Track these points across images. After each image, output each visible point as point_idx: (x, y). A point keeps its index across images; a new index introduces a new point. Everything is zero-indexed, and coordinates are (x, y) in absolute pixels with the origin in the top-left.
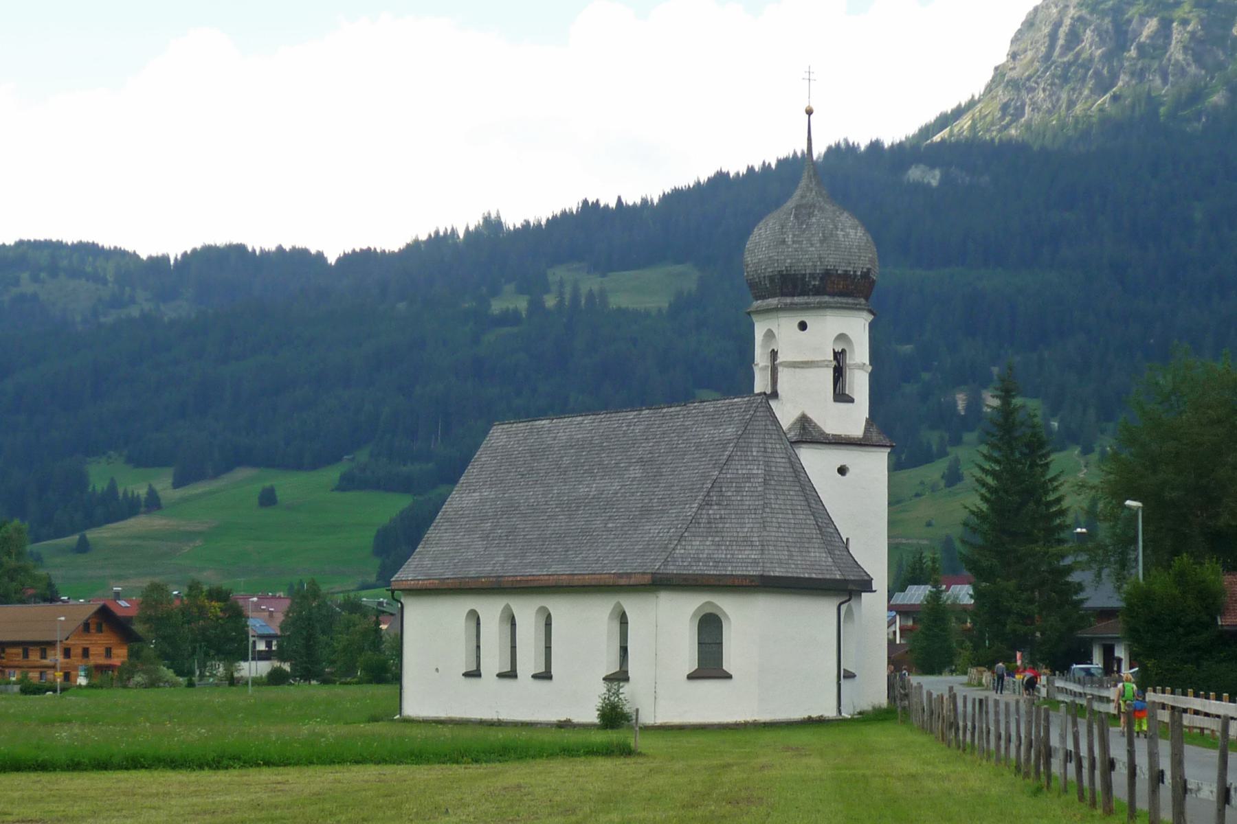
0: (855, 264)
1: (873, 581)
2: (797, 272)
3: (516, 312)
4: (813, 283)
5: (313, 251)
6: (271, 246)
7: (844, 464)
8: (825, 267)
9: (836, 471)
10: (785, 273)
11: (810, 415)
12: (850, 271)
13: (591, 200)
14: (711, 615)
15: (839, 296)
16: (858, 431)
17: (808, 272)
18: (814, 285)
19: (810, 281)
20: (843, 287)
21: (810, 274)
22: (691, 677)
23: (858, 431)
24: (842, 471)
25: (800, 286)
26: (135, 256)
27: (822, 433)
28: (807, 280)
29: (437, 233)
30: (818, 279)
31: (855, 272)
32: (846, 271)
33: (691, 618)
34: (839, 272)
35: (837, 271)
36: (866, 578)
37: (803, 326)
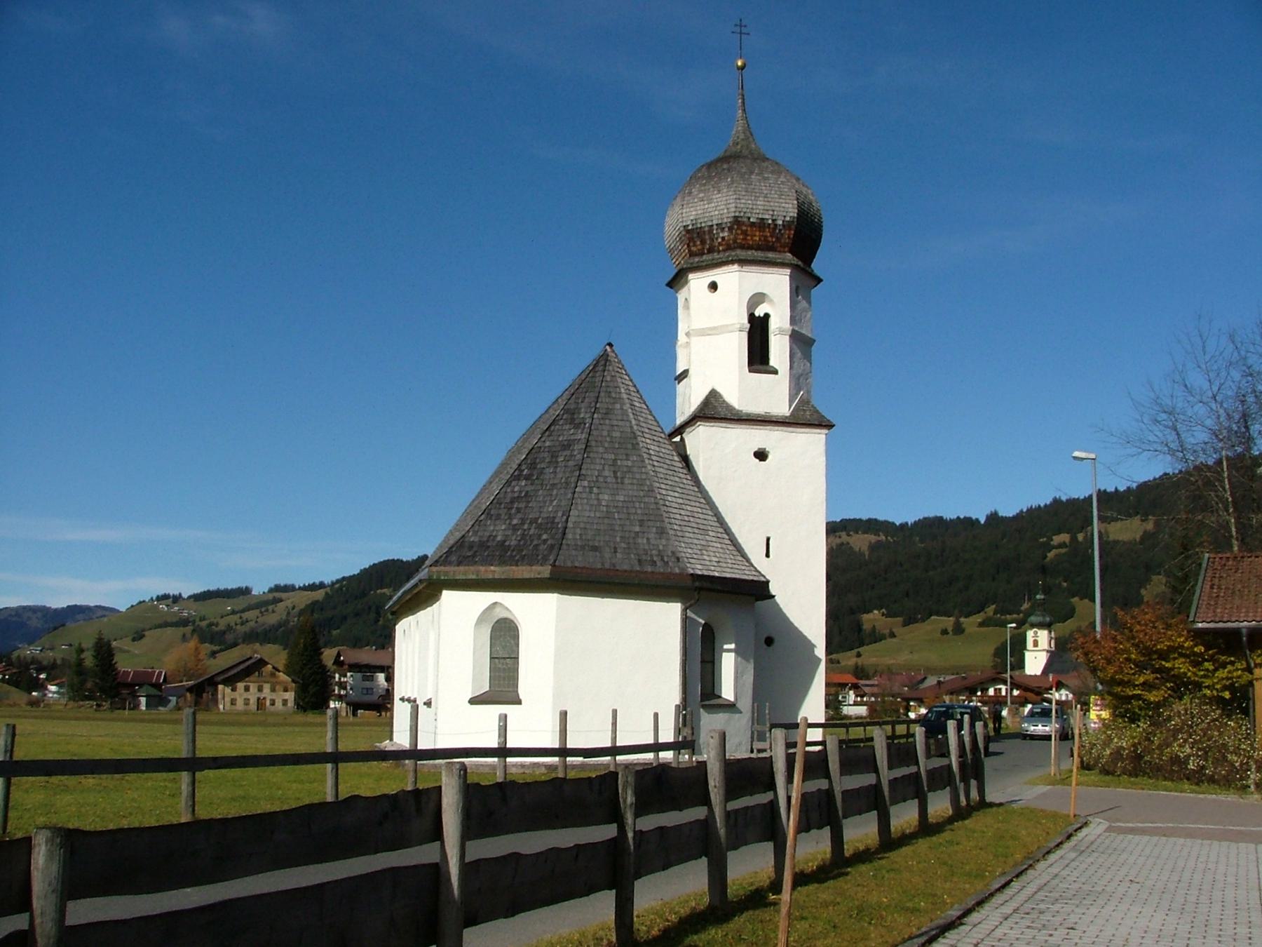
0: (773, 211)
1: (770, 584)
2: (703, 225)
3: (1064, 543)
4: (721, 235)
5: (974, 518)
6: (954, 516)
7: (764, 447)
8: (733, 215)
9: (767, 461)
10: (690, 227)
11: (719, 390)
12: (767, 219)
13: (1102, 489)
14: (505, 619)
15: (756, 250)
16: (782, 408)
17: (715, 222)
18: (723, 238)
19: (718, 233)
20: (760, 239)
21: (717, 225)
22: (474, 701)
23: (782, 408)
24: (761, 455)
25: (708, 242)
26: (893, 524)
27: (729, 407)
28: (715, 232)
29: (1031, 507)
30: (727, 229)
31: (774, 220)
32: (763, 219)
33: (476, 625)
34: (751, 220)
35: (749, 218)
36: (763, 579)
37: (713, 286)
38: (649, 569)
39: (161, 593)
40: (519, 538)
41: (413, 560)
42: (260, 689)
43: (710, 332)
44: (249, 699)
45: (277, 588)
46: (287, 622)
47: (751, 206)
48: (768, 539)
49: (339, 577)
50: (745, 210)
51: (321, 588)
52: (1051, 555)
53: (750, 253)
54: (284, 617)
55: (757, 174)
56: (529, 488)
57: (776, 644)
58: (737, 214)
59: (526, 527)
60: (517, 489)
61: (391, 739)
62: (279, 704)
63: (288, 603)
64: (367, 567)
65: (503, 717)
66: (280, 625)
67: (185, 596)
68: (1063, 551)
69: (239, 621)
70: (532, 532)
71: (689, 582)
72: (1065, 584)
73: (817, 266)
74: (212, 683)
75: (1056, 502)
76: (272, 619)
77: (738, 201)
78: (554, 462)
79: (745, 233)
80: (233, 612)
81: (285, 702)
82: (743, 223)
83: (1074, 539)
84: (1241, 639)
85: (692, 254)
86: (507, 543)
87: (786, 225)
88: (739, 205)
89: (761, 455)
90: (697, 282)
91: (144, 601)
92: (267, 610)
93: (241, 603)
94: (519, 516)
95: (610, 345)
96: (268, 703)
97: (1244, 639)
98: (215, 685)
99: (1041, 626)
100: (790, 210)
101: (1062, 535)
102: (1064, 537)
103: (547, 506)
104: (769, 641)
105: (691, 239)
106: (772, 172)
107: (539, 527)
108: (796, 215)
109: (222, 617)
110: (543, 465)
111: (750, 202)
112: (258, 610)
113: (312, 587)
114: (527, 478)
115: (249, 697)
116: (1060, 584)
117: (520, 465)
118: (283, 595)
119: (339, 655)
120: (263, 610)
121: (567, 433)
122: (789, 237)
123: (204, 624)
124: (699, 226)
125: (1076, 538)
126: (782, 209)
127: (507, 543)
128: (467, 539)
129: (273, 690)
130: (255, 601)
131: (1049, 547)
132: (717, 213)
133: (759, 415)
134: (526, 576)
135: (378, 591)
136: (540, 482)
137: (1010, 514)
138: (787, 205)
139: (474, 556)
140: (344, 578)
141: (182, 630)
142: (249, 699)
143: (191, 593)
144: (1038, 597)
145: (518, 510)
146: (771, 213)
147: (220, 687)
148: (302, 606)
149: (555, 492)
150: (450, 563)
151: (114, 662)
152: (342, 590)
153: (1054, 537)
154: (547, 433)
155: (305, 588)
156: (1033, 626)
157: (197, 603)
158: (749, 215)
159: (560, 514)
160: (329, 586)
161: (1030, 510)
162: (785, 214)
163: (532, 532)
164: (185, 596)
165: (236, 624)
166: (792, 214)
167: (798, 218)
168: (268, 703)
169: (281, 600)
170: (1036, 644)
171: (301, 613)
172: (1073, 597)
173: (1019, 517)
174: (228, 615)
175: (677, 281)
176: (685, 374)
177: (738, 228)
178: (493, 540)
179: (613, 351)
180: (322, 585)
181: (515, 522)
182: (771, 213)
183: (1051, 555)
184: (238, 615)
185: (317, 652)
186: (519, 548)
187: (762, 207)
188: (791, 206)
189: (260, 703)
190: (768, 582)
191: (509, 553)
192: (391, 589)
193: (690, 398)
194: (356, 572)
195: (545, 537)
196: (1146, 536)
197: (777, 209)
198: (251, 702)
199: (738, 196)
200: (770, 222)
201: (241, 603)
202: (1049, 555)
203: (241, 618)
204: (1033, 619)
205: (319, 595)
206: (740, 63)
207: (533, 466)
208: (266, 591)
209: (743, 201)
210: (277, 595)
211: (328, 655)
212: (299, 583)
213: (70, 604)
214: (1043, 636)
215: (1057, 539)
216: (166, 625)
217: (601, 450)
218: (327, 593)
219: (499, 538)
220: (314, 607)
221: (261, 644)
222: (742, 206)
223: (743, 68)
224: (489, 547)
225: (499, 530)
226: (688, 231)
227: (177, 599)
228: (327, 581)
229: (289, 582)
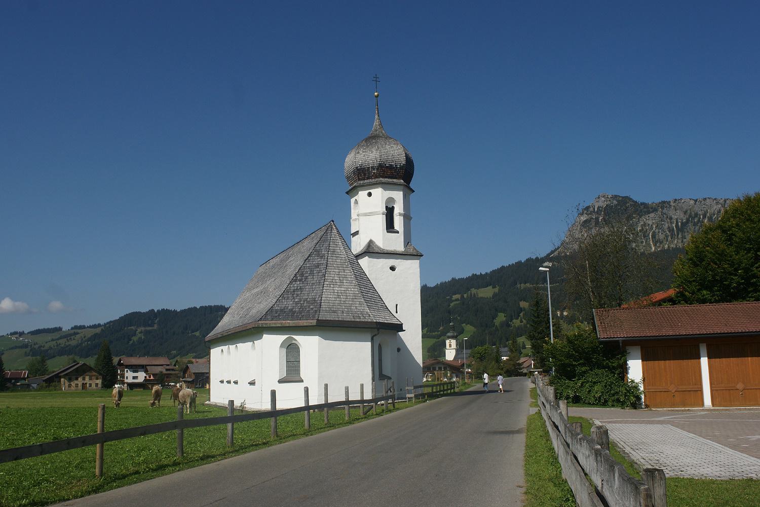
4: (373, 171)
17: (370, 166)
24: (393, 269)
38: (358, 320)
39: (13, 331)
40: (299, 308)
41: (147, 312)
42: (84, 379)
44: (78, 384)
45: (76, 327)
46: (81, 344)
48: (397, 305)
49: (108, 321)
51: (98, 327)
52: (452, 304)
53: (386, 179)
54: (80, 342)
55: (389, 145)
56: (301, 285)
57: (401, 351)
59: (302, 302)
60: (295, 285)
61: (209, 401)
62: (94, 386)
63: (82, 335)
64: (123, 316)
65: (306, 389)
66: (77, 346)
67: (26, 332)
68: (458, 302)
69: (55, 344)
70: (305, 305)
71: (375, 326)
72: (459, 318)
73: (411, 185)
74: (58, 377)
75: (453, 279)
76: (73, 343)
78: (312, 273)
79: (384, 171)
80: (53, 340)
81: (97, 385)
83: (462, 297)
84: (619, 345)
86: (294, 310)
87: (401, 168)
89: (393, 269)
90: (362, 194)
91: (3, 336)
92: (71, 339)
93: (56, 335)
94: (298, 297)
95: (333, 221)
96: (88, 385)
97: (621, 344)
98: (60, 377)
99: (453, 337)
101: (457, 295)
102: (458, 296)
103: (308, 294)
104: (399, 350)
105: (359, 173)
106: (395, 144)
107: (308, 302)
109: (46, 343)
110: (307, 275)
112: (66, 339)
113: (94, 326)
114: (300, 280)
115: (78, 383)
116: (457, 317)
117: (296, 275)
118: (79, 331)
119: (120, 360)
120: (68, 338)
121: (317, 260)
122: (402, 173)
123: (36, 347)
124: (363, 167)
125: (463, 296)
127: (294, 310)
128: (274, 308)
129: (90, 379)
130: (64, 334)
131: (451, 301)
132: (371, 162)
134: (305, 324)
135: (129, 328)
136: (306, 282)
137: (432, 286)
139: (279, 316)
140: (111, 322)
141: (25, 350)
142: (78, 384)
143: (27, 332)
144: (451, 324)
145: (297, 295)
146: (395, 162)
147: (62, 379)
148: (90, 336)
149: (314, 287)
150: (268, 320)
151: (3, 368)
152: (110, 327)
153: (453, 296)
154: (307, 261)
155: (90, 327)
156: (449, 337)
157: (33, 336)
158: (386, 163)
159: (317, 297)
160: (103, 325)
161: (442, 284)
163: (305, 305)
164: (26, 332)
165: (54, 346)
166: (404, 163)
167: (406, 165)
168: (88, 385)
169: (78, 333)
170: (450, 346)
171: (89, 340)
172: (463, 323)
173: (436, 287)
174: (50, 341)
175: (352, 192)
176: (357, 233)
178: (287, 309)
179: (334, 224)
180: (99, 325)
181: (296, 300)
182: (395, 162)
183: (452, 304)
184: (55, 342)
185: (111, 360)
186: (300, 312)
189: (84, 385)
190: (402, 324)
191: (296, 314)
192: (135, 327)
193: (358, 245)
194: (117, 318)
195: (312, 307)
196: (495, 295)
198: (79, 385)
201: (56, 335)
202: (451, 304)
203: (56, 343)
204: (449, 334)
205: (98, 330)
206: (376, 94)
207: (302, 275)
208: (70, 329)
209: (383, 157)
210: (76, 331)
211: (115, 360)
212: (87, 324)
214: (453, 342)
215: (455, 297)
216: (16, 347)
218: (102, 329)
219: (289, 308)
220: (95, 336)
221: (67, 356)
223: (377, 97)
224: (285, 312)
225: (289, 304)
226: (358, 170)
227: (21, 334)
228: (102, 323)
229: (82, 324)
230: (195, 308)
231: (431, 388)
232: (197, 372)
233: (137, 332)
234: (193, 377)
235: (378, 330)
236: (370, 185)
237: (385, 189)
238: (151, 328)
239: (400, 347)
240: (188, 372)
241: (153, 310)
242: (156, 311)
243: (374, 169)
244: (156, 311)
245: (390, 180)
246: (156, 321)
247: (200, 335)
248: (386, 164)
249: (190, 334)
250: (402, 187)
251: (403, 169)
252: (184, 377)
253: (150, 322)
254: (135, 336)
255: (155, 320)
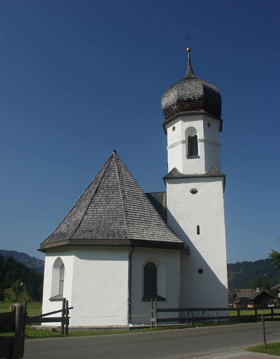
8: (177, 99)
11: (176, 168)
27: (179, 173)
35: (183, 99)
43: (173, 146)
47: (184, 94)
50: (181, 96)
58: (178, 98)
77: (178, 93)
82: (181, 101)
85: (167, 118)
87: (200, 99)
88: (179, 95)
100: (200, 93)
104: (201, 271)
108: (203, 94)
111: (183, 93)
122: (201, 104)
126: (197, 93)
133: (191, 175)
135: (262, 275)
138: (199, 91)
158: (183, 98)
162: (198, 95)
177: (179, 104)
182: (192, 95)
187: (189, 94)
188: (201, 91)
197: (195, 93)
199: (178, 92)
200: (192, 99)
206: (188, 49)
209: (181, 93)
213: (24, 253)
217: (102, 191)
222: (180, 95)
230: (262, 260)
231: (237, 312)
232: (241, 297)
233: (231, 274)
234: (239, 300)
235: (133, 248)
236: (173, 118)
237: (185, 121)
238: (238, 273)
239: (202, 268)
240: (237, 297)
241: (239, 262)
242: (240, 263)
243: (174, 106)
244: (240, 263)
245: (189, 112)
246: (241, 269)
247: (267, 276)
248: (183, 99)
249: (261, 275)
250: (201, 116)
251: (201, 100)
252: (235, 300)
253: (238, 269)
254: (230, 277)
255: (241, 268)
